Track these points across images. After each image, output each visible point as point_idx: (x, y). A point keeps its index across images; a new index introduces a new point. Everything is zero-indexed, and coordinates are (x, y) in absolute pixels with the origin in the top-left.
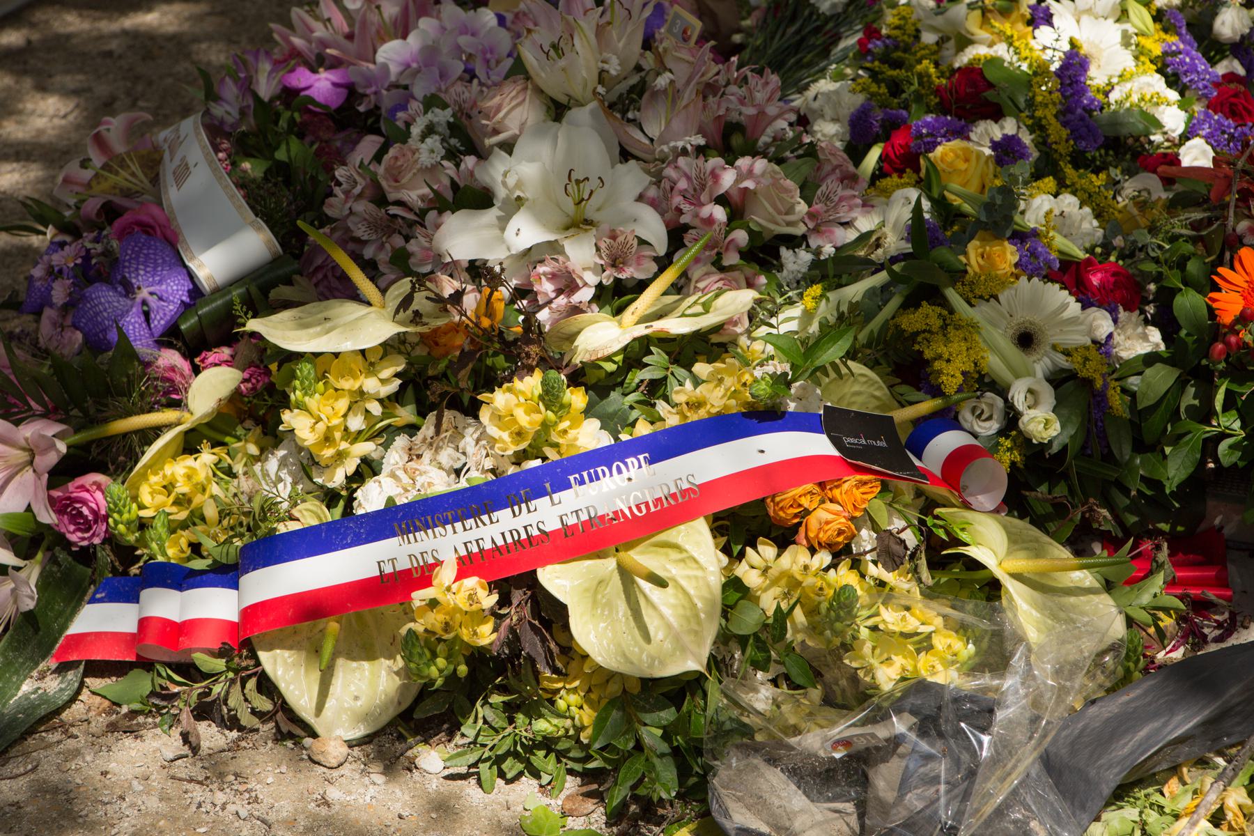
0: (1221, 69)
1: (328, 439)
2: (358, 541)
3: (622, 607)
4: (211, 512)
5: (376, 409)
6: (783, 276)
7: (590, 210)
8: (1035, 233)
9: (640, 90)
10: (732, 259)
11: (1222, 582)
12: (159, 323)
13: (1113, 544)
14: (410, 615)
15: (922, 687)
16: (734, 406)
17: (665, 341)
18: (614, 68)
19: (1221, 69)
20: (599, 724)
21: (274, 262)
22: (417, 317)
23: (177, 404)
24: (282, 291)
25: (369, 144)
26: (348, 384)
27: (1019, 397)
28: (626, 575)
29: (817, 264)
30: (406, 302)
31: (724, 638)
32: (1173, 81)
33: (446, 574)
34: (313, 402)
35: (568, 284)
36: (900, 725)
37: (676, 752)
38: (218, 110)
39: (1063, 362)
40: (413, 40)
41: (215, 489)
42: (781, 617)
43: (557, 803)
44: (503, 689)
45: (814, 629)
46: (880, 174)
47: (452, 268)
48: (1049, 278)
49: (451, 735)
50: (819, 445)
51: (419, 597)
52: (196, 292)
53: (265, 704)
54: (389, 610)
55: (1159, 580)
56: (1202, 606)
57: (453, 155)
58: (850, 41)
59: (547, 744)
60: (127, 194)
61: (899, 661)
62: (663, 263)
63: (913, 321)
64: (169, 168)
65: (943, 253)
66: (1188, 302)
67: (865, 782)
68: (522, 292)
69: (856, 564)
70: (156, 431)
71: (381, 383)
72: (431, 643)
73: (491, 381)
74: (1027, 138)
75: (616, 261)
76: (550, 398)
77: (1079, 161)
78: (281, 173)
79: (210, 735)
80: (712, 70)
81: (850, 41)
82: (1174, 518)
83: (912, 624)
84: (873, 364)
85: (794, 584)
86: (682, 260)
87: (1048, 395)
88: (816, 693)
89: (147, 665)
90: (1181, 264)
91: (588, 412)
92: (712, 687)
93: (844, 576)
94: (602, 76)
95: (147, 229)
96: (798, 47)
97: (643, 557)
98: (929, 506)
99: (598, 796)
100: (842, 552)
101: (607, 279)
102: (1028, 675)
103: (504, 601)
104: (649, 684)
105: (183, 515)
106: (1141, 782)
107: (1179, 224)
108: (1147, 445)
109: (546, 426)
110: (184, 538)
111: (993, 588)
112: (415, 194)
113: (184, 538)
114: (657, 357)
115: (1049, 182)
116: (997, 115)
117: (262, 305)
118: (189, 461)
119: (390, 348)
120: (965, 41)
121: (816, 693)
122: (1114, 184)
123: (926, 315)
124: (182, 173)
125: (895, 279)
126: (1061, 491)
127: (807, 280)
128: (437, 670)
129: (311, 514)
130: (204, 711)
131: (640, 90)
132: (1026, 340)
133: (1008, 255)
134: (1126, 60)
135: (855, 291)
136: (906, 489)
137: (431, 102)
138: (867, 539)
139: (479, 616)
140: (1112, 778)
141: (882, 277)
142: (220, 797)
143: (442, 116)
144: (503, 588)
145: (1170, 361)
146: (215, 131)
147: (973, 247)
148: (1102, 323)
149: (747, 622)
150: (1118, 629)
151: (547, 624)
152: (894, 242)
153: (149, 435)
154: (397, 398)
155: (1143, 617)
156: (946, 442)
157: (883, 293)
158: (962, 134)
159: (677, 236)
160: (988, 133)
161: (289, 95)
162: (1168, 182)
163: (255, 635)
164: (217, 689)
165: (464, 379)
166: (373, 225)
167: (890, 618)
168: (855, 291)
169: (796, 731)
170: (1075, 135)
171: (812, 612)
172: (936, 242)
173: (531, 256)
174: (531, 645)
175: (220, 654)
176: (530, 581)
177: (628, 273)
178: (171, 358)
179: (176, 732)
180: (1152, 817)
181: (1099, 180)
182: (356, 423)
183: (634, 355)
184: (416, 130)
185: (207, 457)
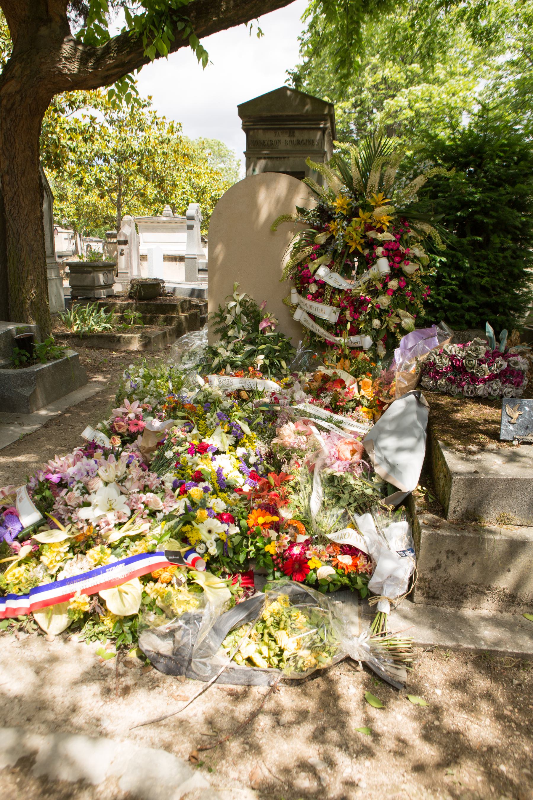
0: (251, 469)
1: (51, 562)
2: (58, 587)
3: (119, 600)
4: (24, 581)
5: (63, 555)
6: (157, 519)
7: (113, 507)
8: (211, 508)
9: (125, 478)
10: (145, 516)
11: (252, 583)
12: (13, 535)
13: (230, 575)
14: (69, 604)
15: (186, 613)
16: (144, 551)
17: (129, 537)
18: (119, 474)
19: (251, 469)
20: (114, 626)
21: (41, 520)
22: (73, 533)
23: (17, 554)
24: (41, 528)
25: (65, 490)
26: (56, 550)
27: (208, 545)
28: (120, 592)
29: (165, 516)
30: (70, 530)
31: (143, 605)
32: (241, 472)
33: (78, 594)
34: (47, 554)
35: (108, 524)
36: (181, 623)
37: (132, 632)
38: (30, 484)
39: (218, 536)
40: (76, 467)
41: (25, 575)
42: (154, 600)
43: (104, 646)
44: (92, 620)
45: (163, 601)
46: (179, 495)
47: (82, 521)
48: (215, 517)
49: (80, 631)
50: (163, 559)
51: (71, 600)
52: (22, 528)
53: (35, 627)
54: (65, 603)
55: (238, 585)
56: (248, 589)
57: (83, 494)
58: (173, 464)
59: (102, 633)
60: (8, 504)
61: (183, 606)
62: (130, 518)
63: (185, 529)
64: (18, 498)
65: (192, 513)
66: (243, 522)
67: (174, 636)
68: (98, 526)
69: (172, 585)
70: (11, 562)
71: (66, 547)
72: (74, 611)
73: (89, 547)
74: (210, 486)
75: (119, 518)
76: (102, 551)
77: (222, 491)
78: (44, 498)
79: (22, 635)
80: (142, 473)
81: (173, 464)
82: (243, 569)
83: (186, 598)
84: (176, 539)
85: (158, 592)
86: (134, 517)
87: (215, 544)
88: (164, 615)
89: (7, 619)
90: (242, 513)
91: (111, 554)
92: (140, 616)
93: (170, 588)
94: (116, 476)
95: (12, 513)
96: (162, 466)
97: (123, 587)
98: (189, 571)
99: (114, 644)
100: (169, 583)
101: (117, 522)
102: (209, 609)
103: (92, 599)
104: (125, 617)
105: (17, 581)
106: (234, 630)
107: (242, 505)
108: (236, 552)
109: (101, 558)
110: (17, 587)
111: (202, 590)
112: (73, 503)
113: (17, 587)
114: (127, 540)
115: (215, 496)
116: (204, 481)
117: (35, 532)
118: (19, 568)
119: (66, 540)
120: (197, 465)
121: (164, 615)
122: (229, 496)
123: (188, 527)
124: (21, 499)
125: (181, 520)
126: (218, 565)
127: (163, 520)
128: (76, 617)
129: (48, 581)
130: (21, 629)
131: (125, 478)
132: (210, 532)
133: (206, 512)
134: (231, 468)
135: (172, 523)
136: (183, 568)
137: (79, 482)
138: (174, 581)
139: (85, 604)
140: (227, 630)
141: (178, 519)
142: (24, 651)
143: (81, 485)
144: (92, 597)
145: (241, 535)
146: (29, 489)
147: (198, 511)
148: (225, 527)
149: (148, 601)
150: (230, 596)
151: (102, 604)
152: (182, 511)
153: (10, 562)
154: (68, 552)
155: (235, 592)
156: (192, 556)
157: (179, 522)
158: (196, 486)
159: (133, 511)
160: (202, 485)
161: (47, 480)
162: (240, 495)
163: (33, 610)
164: (24, 624)
165: (83, 547)
166: (64, 510)
167: (181, 597)
168: (172, 523)
169: (158, 625)
170: (220, 485)
171: (162, 597)
172: (190, 511)
173: (100, 518)
174: (98, 610)
175: (26, 615)
176: (97, 594)
177: (122, 520)
178: (16, 544)
179: (14, 635)
180: (237, 638)
181: (226, 495)
182: (58, 558)
183: (122, 541)
184: (74, 489)
185: (24, 567)
